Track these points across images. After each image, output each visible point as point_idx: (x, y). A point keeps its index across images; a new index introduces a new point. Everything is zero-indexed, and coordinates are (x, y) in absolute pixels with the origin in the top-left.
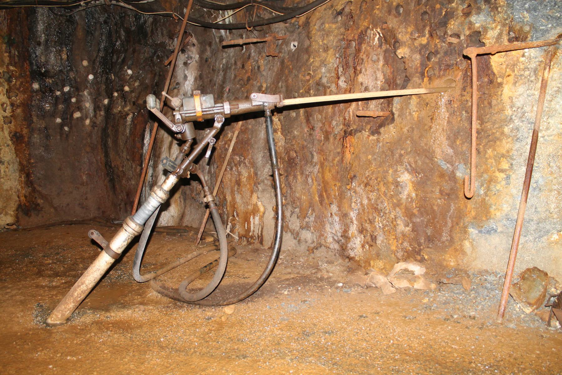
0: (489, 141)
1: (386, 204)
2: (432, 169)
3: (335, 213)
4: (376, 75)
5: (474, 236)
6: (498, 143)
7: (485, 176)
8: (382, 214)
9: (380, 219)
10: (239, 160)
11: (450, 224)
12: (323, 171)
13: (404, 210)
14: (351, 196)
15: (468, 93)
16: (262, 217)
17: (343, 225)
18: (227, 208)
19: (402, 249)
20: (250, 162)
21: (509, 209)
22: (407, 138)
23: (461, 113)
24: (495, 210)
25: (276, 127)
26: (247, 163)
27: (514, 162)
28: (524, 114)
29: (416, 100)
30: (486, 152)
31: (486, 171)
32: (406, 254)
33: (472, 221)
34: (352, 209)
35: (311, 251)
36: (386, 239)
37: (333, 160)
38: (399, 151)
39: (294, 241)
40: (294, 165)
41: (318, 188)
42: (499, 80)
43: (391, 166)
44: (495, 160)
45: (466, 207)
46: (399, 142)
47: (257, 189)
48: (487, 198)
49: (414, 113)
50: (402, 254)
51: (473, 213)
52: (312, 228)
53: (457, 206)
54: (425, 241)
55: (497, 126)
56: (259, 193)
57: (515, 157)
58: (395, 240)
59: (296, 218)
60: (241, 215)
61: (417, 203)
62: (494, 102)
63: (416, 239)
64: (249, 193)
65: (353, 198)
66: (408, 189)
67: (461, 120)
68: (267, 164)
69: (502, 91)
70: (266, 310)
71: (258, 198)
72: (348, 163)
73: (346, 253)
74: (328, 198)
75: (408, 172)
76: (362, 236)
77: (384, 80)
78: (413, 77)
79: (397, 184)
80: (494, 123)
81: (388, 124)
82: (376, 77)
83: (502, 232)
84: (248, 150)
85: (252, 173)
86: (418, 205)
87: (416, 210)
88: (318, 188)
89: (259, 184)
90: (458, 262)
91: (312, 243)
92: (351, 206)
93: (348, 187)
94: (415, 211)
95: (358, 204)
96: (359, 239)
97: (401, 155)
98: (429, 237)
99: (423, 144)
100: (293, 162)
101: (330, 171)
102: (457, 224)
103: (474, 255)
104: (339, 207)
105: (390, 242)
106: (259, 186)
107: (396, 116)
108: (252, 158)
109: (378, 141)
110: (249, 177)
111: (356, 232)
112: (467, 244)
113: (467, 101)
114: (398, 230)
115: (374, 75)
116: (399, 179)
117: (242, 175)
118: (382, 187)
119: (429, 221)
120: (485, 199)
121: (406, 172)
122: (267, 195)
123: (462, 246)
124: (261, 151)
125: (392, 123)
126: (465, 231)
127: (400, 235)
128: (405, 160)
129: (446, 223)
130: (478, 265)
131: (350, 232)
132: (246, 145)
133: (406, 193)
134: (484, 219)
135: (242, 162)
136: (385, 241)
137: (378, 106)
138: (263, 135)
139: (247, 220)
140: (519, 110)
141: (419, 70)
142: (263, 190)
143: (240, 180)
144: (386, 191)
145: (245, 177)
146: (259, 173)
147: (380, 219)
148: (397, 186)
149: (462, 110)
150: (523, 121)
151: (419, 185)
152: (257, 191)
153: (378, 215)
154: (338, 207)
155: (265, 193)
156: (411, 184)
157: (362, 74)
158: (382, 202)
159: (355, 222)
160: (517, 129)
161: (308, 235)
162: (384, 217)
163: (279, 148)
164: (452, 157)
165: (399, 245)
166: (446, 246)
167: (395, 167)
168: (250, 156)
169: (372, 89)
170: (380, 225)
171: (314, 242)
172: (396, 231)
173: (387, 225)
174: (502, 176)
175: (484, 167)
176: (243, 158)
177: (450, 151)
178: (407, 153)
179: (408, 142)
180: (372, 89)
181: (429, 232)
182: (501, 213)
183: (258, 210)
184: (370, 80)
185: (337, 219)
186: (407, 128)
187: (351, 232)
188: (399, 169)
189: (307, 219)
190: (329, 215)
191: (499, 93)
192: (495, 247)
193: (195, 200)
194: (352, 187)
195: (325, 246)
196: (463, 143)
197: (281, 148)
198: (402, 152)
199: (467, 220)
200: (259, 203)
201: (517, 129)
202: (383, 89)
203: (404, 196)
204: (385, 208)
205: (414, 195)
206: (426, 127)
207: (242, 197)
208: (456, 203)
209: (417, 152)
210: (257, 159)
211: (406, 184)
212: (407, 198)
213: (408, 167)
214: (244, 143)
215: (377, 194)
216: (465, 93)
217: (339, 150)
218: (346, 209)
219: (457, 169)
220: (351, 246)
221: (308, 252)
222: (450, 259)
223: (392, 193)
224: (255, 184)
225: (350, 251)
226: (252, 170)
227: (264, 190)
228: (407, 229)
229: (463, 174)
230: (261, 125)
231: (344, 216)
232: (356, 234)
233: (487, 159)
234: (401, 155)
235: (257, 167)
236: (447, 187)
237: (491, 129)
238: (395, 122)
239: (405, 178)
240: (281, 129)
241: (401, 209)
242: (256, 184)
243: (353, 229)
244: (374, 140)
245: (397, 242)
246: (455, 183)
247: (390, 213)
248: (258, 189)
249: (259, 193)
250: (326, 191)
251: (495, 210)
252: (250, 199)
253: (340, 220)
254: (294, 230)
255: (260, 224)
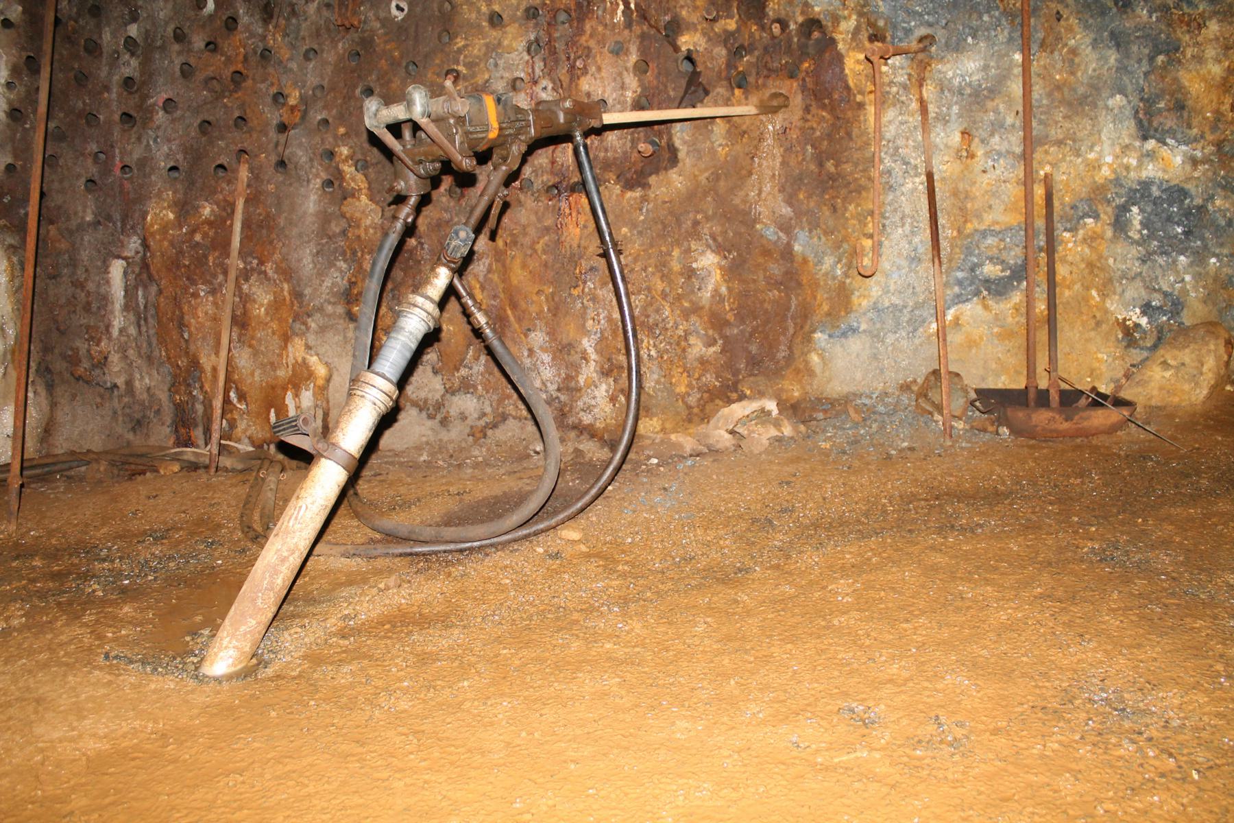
0: (851, 192)
1: (667, 313)
2: (750, 243)
3: (541, 348)
4: (622, 79)
5: (823, 344)
6: (864, 194)
7: (845, 246)
8: (658, 332)
9: (651, 342)
10: (245, 268)
11: (791, 331)
12: (504, 266)
13: (706, 318)
14: (584, 308)
15: (813, 116)
16: (322, 391)
17: (563, 367)
18: (202, 388)
19: (699, 389)
20: (278, 270)
21: (880, 293)
22: (705, 194)
23: (804, 150)
24: (859, 297)
25: (353, 184)
26: (270, 273)
27: (887, 222)
28: (897, 149)
29: (722, 125)
30: (846, 209)
31: (845, 239)
32: (706, 395)
33: (824, 319)
34: (587, 333)
35: (478, 435)
36: (665, 376)
37: (534, 243)
38: (691, 215)
39: (429, 423)
40: (411, 263)
41: (493, 302)
42: (859, 98)
43: (678, 243)
44: (860, 221)
45: (815, 298)
46: (692, 196)
47: (303, 327)
48: (848, 281)
49: (720, 149)
50: (699, 396)
51: (826, 308)
52: (480, 387)
53: (800, 298)
54: (747, 366)
55: (861, 168)
56: (311, 338)
57: (887, 215)
58: (685, 374)
59: (431, 374)
60: (254, 394)
61: (733, 303)
62: (855, 132)
63: (730, 366)
64: (276, 342)
65: (589, 311)
66: (713, 281)
67: (804, 160)
68: (330, 268)
69: (865, 115)
70: (418, 563)
71: (308, 347)
72: (575, 245)
73: (571, 420)
74: (519, 320)
75: (713, 251)
76: (611, 380)
77: (639, 90)
78: (715, 87)
79: (690, 273)
80: (856, 165)
81: (666, 169)
82: (623, 83)
83: (865, 331)
84: (271, 243)
85: (286, 293)
86: (735, 306)
87: (730, 314)
88: (493, 302)
89: (309, 316)
90: (804, 389)
91: (479, 418)
92: (584, 326)
93: (575, 292)
94: (730, 317)
95: (602, 322)
96: (604, 387)
97: (696, 223)
98: (753, 357)
99: (737, 201)
100: (410, 258)
101: (524, 266)
102: (802, 327)
103: (827, 374)
104: (552, 333)
105: (674, 380)
106: (309, 320)
107: (681, 155)
108: (284, 259)
109: (644, 199)
110: (276, 305)
111: (595, 375)
112: (814, 358)
113: (812, 128)
114: (690, 357)
115: (618, 78)
116: (694, 265)
117: (254, 301)
118: (659, 282)
119: (755, 330)
120: (844, 283)
121: (709, 252)
122: (336, 338)
123: (807, 362)
124: (309, 242)
125: (672, 168)
126: (808, 339)
127: (696, 364)
128: (706, 231)
129: (786, 329)
130: (836, 388)
131: (582, 380)
132: (264, 231)
133: (710, 287)
134: (843, 313)
135: (253, 269)
136: (663, 380)
137: (626, 138)
138: (311, 205)
139: (273, 399)
140: (890, 145)
141: (724, 74)
142: (320, 327)
143: (245, 313)
144: (667, 290)
145: (262, 305)
146: (307, 291)
147: (651, 342)
148: (690, 277)
149: (806, 144)
150: (896, 161)
151: (733, 271)
152: (304, 334)
153: (648, 336)
154: (548, 334)
155: (329, 335)
156: (719, 272)
157: (589, 76)
158: (657, 311)
159: (593, 356)
160: (889, 172)
161: (469, 403)
162: (661, 337)
163: (366, 230)
164: (791, 219)
165: (694, 382)
166: (782, 368)
167: (685, 244)
168: (277, 256)
169: (614, 106)
170: (653, 353)
171: (484, 414)
172: (685, 358)
173: (667, 351)
174: (868, 243)
175: (843, 232)
176: (255, 262)
177: (786, 211)
178: (708, 219)
179: (709, 199)
180: (614, 106)
181: (754, 349)
182: (869, 301)
183: (311, 375)
184: (609, 90)
185: (547, 358)
186: (706, 174)
187: (585, 377)
188: (693, 247)
189: (463, 372)
190: (526, 354)
191: (862, 118)
192: (858, 355)
193: (87, 382)
194: (587, 290)
195: (515, 418)
196: (809, 197)
197: (371, 231)
198: (699, 217)
199: (816, 318)
200: (313, 360)
201: (889, 172)
202: (638, 106)
203: (706, 295)
204: (663, 320)
205: (724, 290)
206: (744, 172)
207: (256, 353)
208: (799, 295)
209: (725, 216)
210: (299, 260)
211: (710, 272)
212: (713, 296)
213: (711, 242)
214: (254, 226)
215: (647, 297)
216: (809, 117)
217: (549, 222)
218: (572, 335)
219: (795, 240)
220: (585, 404)
221: (471, 438)
222: (791, 387)
223: (680, 291)
224: (296, 318)
225: (582, 414)
226: (286, 286)
227: (322, 330)
228: (712, 349)
229: (804, 246)
230: (305, 183)
231: (564, 351)
232: (596, 379)
233: (847, 219)
234: (696, 223)
235: (300, 280)
236: (776, 269)
237: (851, 173)
238: (680, 165)
239: (708, 261)
240: (369, 189)
241: (701, 317)
242: (301, 316)
243: (589, 371)
244: (635, 199)
245: (689, 376)
246: (792, 262)
247: (676, 326)
248: (308, 328)
249: (311, 338)
250: (514, 306)
251: (859, 297)
252: (280, 355)
253: (553, 359)
254: (426, 401)
255: (316, 406)
